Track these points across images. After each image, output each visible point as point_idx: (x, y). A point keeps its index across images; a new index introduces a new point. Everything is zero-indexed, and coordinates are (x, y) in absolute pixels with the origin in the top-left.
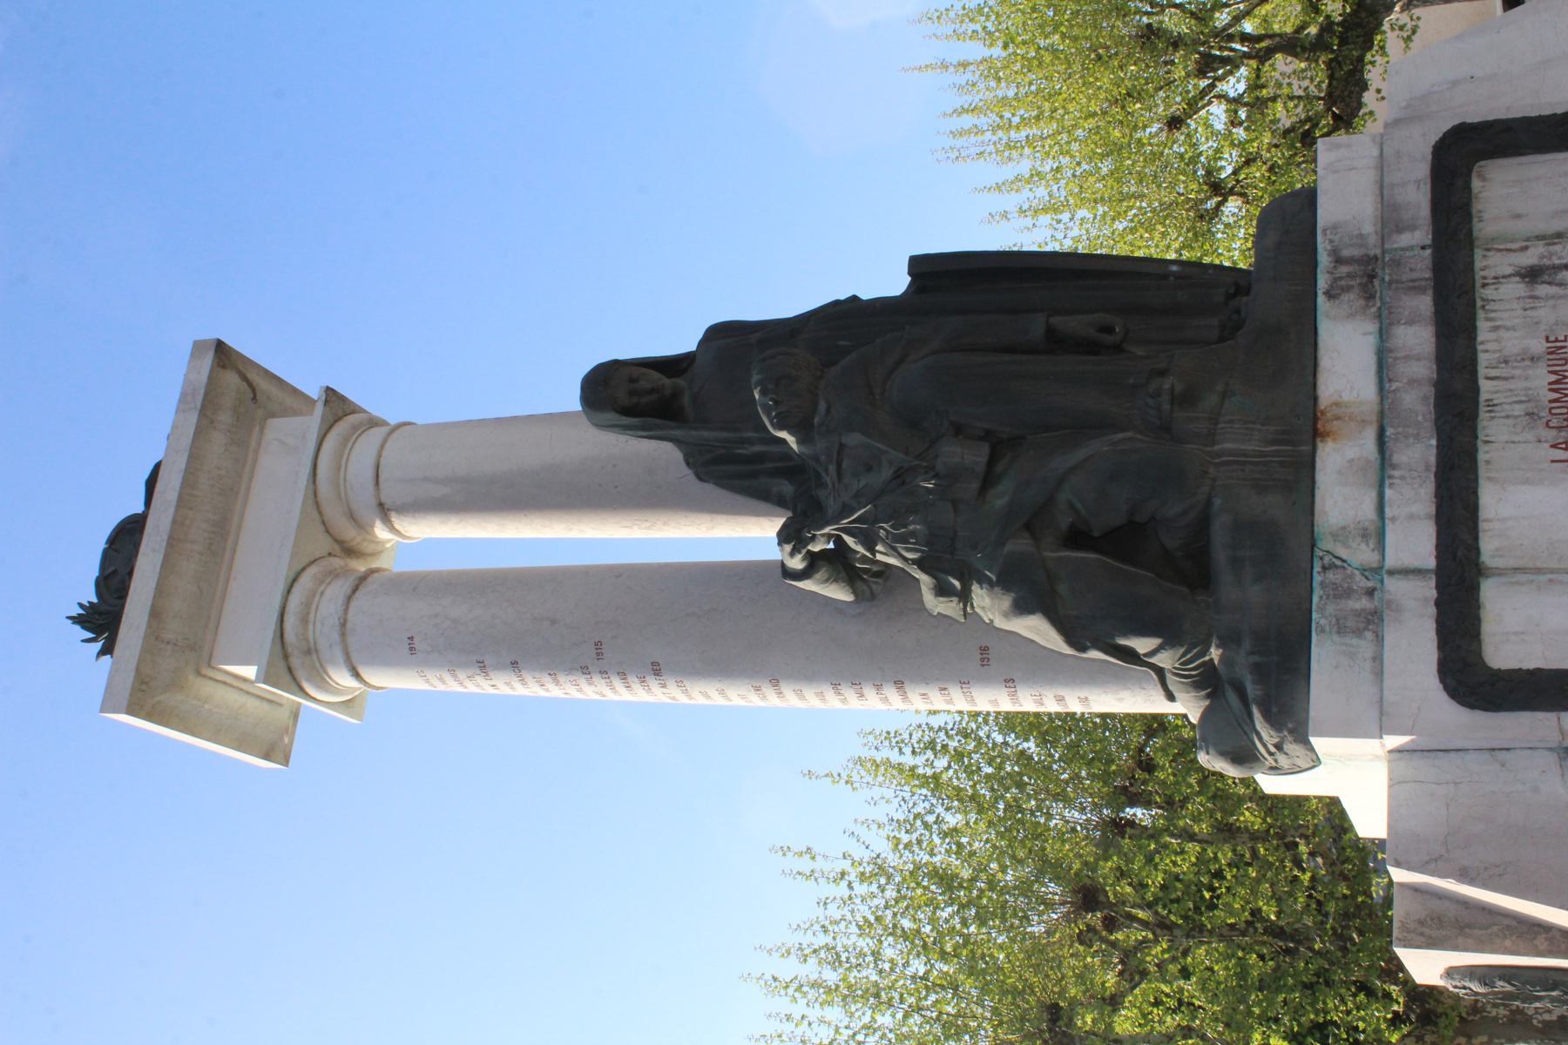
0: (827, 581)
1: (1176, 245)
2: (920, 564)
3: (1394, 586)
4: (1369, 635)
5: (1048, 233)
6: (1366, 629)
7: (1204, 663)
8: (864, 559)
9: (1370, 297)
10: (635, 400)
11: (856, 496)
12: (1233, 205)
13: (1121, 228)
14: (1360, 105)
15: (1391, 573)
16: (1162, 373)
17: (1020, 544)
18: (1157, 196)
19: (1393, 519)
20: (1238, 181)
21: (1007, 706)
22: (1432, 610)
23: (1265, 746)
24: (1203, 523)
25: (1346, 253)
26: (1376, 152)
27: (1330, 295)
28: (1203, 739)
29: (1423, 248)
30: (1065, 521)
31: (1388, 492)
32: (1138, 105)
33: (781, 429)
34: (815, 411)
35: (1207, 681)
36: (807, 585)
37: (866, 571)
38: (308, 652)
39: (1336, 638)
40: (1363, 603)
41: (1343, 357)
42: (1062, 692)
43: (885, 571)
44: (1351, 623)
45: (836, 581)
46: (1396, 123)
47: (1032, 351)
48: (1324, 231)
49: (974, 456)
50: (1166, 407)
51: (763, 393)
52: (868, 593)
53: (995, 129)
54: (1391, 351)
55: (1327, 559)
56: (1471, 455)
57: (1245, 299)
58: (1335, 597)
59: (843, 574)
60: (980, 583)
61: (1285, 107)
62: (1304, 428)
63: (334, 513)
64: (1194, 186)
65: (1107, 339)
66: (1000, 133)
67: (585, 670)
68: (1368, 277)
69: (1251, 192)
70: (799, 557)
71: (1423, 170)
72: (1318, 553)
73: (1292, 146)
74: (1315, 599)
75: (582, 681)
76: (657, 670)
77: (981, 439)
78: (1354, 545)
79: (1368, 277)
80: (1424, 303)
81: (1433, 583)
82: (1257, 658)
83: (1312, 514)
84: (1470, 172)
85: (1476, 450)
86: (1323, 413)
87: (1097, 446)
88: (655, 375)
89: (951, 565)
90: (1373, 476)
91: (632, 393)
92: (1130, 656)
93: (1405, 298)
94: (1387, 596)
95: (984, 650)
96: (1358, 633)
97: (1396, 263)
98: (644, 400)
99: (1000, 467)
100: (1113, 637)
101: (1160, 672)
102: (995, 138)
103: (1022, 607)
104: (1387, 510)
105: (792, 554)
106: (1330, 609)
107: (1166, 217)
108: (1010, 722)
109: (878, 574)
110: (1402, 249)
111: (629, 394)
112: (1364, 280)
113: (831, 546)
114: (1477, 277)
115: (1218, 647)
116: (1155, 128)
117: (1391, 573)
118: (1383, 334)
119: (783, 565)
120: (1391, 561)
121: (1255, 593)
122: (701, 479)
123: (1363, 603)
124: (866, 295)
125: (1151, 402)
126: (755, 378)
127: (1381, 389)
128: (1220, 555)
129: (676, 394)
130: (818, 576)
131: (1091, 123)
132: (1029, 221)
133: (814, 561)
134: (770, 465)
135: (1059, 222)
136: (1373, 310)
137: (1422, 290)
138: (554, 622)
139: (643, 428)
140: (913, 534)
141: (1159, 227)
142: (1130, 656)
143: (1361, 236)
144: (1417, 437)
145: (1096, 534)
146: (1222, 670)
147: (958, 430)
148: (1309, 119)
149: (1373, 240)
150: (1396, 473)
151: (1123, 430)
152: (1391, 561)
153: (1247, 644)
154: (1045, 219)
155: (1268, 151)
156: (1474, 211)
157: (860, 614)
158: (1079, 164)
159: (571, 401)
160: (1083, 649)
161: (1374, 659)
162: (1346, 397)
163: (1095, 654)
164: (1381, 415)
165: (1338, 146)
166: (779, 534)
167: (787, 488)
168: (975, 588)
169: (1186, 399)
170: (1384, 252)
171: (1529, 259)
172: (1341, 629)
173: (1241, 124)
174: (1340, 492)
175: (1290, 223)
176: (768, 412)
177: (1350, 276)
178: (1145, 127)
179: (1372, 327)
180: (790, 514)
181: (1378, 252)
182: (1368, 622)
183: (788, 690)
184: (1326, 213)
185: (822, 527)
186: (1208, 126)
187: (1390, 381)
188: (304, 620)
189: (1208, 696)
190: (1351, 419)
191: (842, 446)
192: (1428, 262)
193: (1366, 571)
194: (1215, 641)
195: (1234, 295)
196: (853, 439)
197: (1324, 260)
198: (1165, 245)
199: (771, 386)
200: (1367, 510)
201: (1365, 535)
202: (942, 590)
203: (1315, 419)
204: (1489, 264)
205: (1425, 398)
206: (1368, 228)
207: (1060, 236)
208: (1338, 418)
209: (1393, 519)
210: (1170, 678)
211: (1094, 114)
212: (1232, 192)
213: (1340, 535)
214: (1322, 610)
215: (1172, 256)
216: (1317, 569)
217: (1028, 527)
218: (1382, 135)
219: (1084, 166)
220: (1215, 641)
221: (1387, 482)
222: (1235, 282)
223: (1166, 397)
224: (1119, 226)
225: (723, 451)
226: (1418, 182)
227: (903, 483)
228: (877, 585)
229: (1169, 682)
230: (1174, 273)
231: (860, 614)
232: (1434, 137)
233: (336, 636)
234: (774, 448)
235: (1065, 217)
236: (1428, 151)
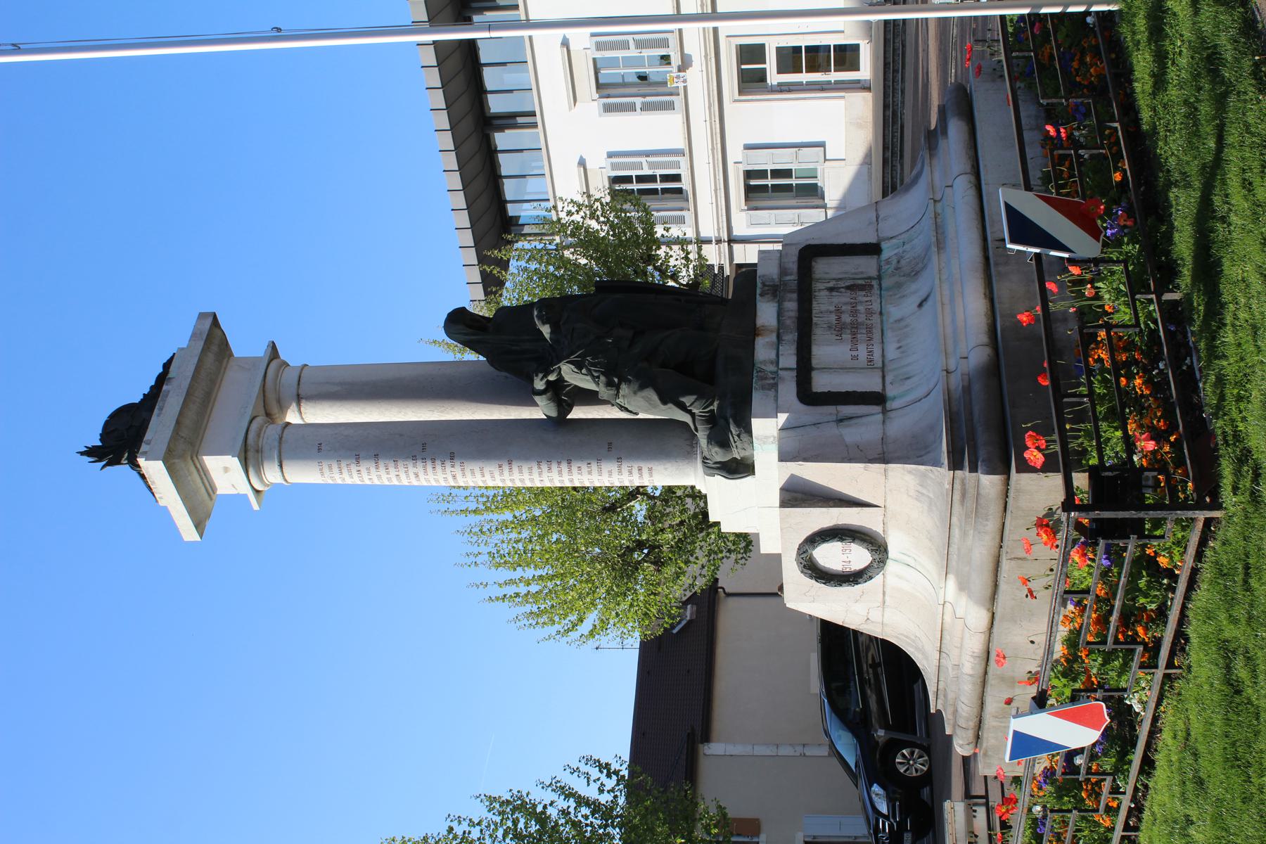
27: (761, 295)
38: (257, 451)
63: (271, 396)
67: (414, 458)
71: (795, 259)
79: (775, 291)
80: (795, 296)
171: (831, 285)
172: (763, 388)
174: (763, 351)
184: (759, 273)
188: (258, 435)
197: (759, 285)
201: (772, 363)
204: (818, 286)
206: (775, 277)
213: (764, 362)
233: (276, 444)
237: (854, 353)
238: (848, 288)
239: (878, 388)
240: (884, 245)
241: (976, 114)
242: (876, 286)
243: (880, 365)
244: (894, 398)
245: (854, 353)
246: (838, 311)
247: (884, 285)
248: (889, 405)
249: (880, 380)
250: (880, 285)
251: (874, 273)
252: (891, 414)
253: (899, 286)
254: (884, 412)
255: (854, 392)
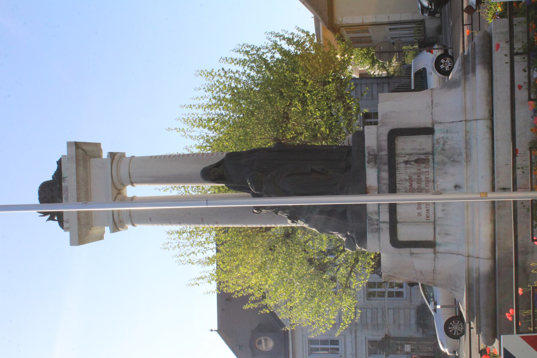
27: (368, 163)
38: (121, 222)
171: (406, 159)
172: (372, 232)
197: (367, 154)
201: (376, 213)
213: (372, 213)
237: (419, 211)
238: (416, 161)
239: (431, 239)
240: (436, 128)
241: (494, 73)
242: (431, 160)
243: (432, 220)
244: (440, 245)
245: (419, 211)
246: (411, 180)
247: (436, 160)
248: (439, 249)
249: (432, 231)
250: (433, 159)
251: (429, 150)
252: (437, 254)
253: (444, 164)
254: (435, 253)
255: (419, 247)
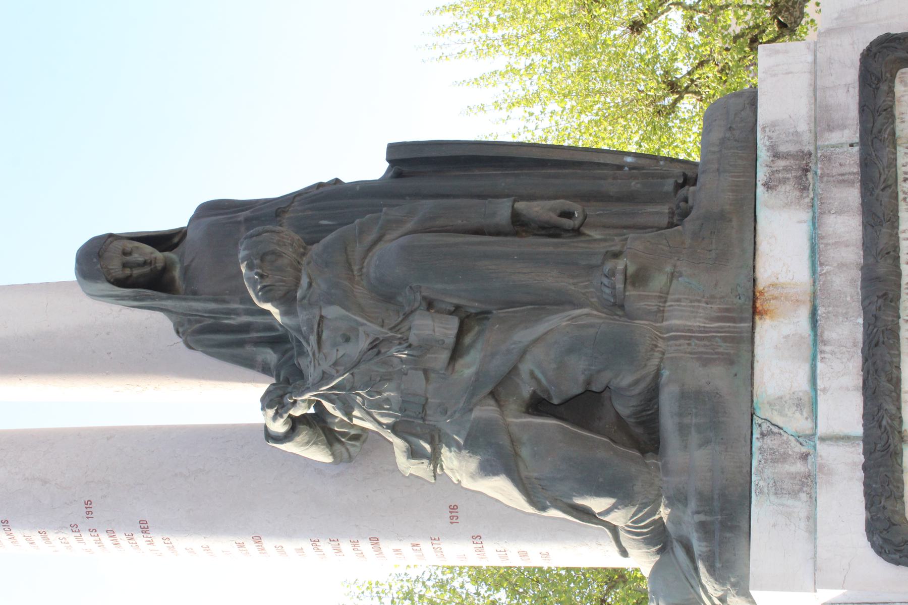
0: (308, 443)
1: (636, 138)
2: (394, 428)
3: (825, 451)
4: (803, 496)
5: (523, 123)
6: (801, 490)
7: (654, 522)
8: (342, 423)
9: (804, 188)
10: (128, 272)
11: (335, 364)
12: (688, 104)
13: (586, 121)
14: (802, 15)
15: (823, 439)
16: (616, 255)
17: (487, 411)
18: (620, 93)
19: (824, 390)
20: (692, 81)
21: (474, 560)
22: (861, 474)
23: (710, 598)
24: (653, 393)
25: (783, 149)
26: (810, 58)
27: (768, 186)
28: (654, 592)
29: (852, 145)
30: (527, 390)
31: (820, 366)
32: (603, 10)
33: (266, 301)
34: (297, 284)
35: (659, 538)
36: (288, 447)
37: (344, 434)
39: (772, 498)
40: (799, 467)
41: (784, 242)
42: (502, 546)
43: (360, 436)
44: (787, 485)
45: (315, 443)
46: (829, 32)
47: (498, 232)
48: (764, 128)
49: (447, 328)
50: (620, 286)
51: (250, 267)
52: (345, 455)
53: (473, 27)
54: (823, 238)
55: (765, 426)
56: (894, 333)
57: (692, 188)
58: (774, 461)
59: (323, 437)
60: (449, 446)
61: (735, 13)
62: (750, 306)
64: (653, 84)
65: (567, 223)
66: (479, 33)
68: (803, 169)
69: (704, 90)
70: (281, 421)
71: (852, 75)
72: (757, 420)
73: (742, 50)
74: (755, 463)
75: (71, 537)
76: (144, 527)
77: (451, 313)
78: (789, 414)
79: (803, 169)
80: (853, 195)
81: (861, 450)
82: (702, 517)
83: (752, 385)
84: (893, 77)
85: (899, 328)
86: (761, 293)
87: (558, 321)
88: (148, 249)
89: (420, 429)
90: (807, 352)
91: (125, 265)
92: (586, 514)
93: (835, 190)
94: (819, 461)
95: (453, 508)
96: (794, 494)
97: (828, 159)
98: (136, 272)
99: (467, 340)
100: (571, 497)
101: (614, 530)
102: (613, 33)
103: (487, 469)
104: (819, 382)
105: (275, 418)
106: (768, 472)
107: (627, 113)
108: (479, 575)
109: (356, 438)
110: (833, 146)
111: (132, 267)
112: (800, 173)
113: (312, 410)
114: (899, 172)
115: (666, 506)
116: (619, 30)
117: (823, 439)
118: (815, 223)
119: (266, 427)
120: (822, 430)
121: (701, 457)
122: (190, 348)
123: (799, 467)
124: (348, 178)
125: (606, 281)
126: (242, 254)
127: (814, 272)
128: (668, 422)
129: (167, 268)
130: (298, 439)
131: (561, 25)
132: (504, 114)
133: (295, 424)
134: (255, 335)
135: (531, 114)
136: (807, 200)
137: (851, 183)
138: (45, 482)
139: (135, 299)
140: (387, 400)
141: (621, 120)
142: (586, 514)
143: (796, 133)
144: (846, 316)
145: (555, 401)
146: (670, 527)
147: (430, 305)
148: (757, 26)
149: (807, 137)
150: (827, 349)
151: (581, 306)
152: (822, 430)
153: (693, 504)
154: (518, 111)
155: (720, 53)
156: (897, 113)
157: (338, 475)
158: (550, 62)
159: (68, 272)
160: (543, 508)
161: (808, 518)
162: (782, 279)
163: (554, 513)
164: (814, 295)
165: (777, 52)
166: (263, 399)
167: (270, 356)
168: (444, 450)
169: (638, 279)
170: (816, 149)
172: (778, 490)
173: (696, 28)
175: (735, 120)
176: (254, 284)
177: (786, 169)
178: (610, 29)
179: (805, 215)
180: (274, 381)
181: (812, 148)
182: (803, 484)
183: (388, 546)
184: (765, 113)
185: (302, 393)
186: (666, 31)
187: (822, 264)
189: (659, 552)
190: (786, 298)
191: (322, 317)
192: (857, 158)
193: (799, 438)
194: (664, 500)
195: (682, 186)
196: (333, 312)
197: (763, 154)
198: (629, 139)
199: (257, 262)
200: (802, 383)
201: (799, 405)
202: (414, 453)
203: (754, 299)
205: (853, 281)
206: (803, 127)
207: (531, 126)
208: (775, 298)
209: (824, 390)
210: (624, 537)
211: (563, 17)
212: (687, 90)
213: (778, 403)
214: (761, 472)
215: (633, 148)
216: (756, 435)
217: (493, 394)
218: (816, 43)
219: (555, 64)
220: (664, 500)
221: (819, 357)
222: (687, 175)
223: (619, 277)
224: (585, 118)
225: (211, 321)
226: (847, 86)
227: (379, 353)
228: (354, 448)
229: (621, 539)
230: (628, 164)
231: (338, 475)
232: (863, 46)
234: (259, 319)
235: (537, 109)
236: (856, 58)
